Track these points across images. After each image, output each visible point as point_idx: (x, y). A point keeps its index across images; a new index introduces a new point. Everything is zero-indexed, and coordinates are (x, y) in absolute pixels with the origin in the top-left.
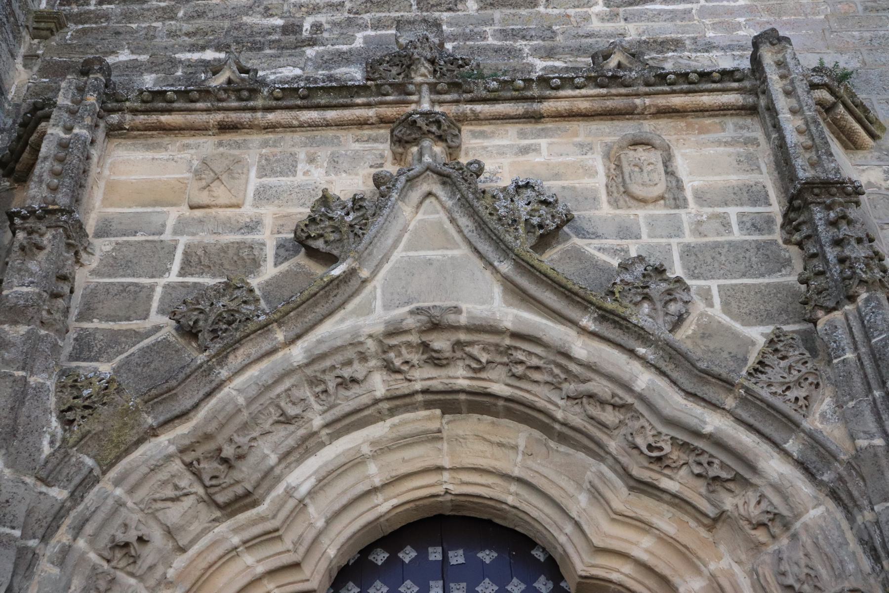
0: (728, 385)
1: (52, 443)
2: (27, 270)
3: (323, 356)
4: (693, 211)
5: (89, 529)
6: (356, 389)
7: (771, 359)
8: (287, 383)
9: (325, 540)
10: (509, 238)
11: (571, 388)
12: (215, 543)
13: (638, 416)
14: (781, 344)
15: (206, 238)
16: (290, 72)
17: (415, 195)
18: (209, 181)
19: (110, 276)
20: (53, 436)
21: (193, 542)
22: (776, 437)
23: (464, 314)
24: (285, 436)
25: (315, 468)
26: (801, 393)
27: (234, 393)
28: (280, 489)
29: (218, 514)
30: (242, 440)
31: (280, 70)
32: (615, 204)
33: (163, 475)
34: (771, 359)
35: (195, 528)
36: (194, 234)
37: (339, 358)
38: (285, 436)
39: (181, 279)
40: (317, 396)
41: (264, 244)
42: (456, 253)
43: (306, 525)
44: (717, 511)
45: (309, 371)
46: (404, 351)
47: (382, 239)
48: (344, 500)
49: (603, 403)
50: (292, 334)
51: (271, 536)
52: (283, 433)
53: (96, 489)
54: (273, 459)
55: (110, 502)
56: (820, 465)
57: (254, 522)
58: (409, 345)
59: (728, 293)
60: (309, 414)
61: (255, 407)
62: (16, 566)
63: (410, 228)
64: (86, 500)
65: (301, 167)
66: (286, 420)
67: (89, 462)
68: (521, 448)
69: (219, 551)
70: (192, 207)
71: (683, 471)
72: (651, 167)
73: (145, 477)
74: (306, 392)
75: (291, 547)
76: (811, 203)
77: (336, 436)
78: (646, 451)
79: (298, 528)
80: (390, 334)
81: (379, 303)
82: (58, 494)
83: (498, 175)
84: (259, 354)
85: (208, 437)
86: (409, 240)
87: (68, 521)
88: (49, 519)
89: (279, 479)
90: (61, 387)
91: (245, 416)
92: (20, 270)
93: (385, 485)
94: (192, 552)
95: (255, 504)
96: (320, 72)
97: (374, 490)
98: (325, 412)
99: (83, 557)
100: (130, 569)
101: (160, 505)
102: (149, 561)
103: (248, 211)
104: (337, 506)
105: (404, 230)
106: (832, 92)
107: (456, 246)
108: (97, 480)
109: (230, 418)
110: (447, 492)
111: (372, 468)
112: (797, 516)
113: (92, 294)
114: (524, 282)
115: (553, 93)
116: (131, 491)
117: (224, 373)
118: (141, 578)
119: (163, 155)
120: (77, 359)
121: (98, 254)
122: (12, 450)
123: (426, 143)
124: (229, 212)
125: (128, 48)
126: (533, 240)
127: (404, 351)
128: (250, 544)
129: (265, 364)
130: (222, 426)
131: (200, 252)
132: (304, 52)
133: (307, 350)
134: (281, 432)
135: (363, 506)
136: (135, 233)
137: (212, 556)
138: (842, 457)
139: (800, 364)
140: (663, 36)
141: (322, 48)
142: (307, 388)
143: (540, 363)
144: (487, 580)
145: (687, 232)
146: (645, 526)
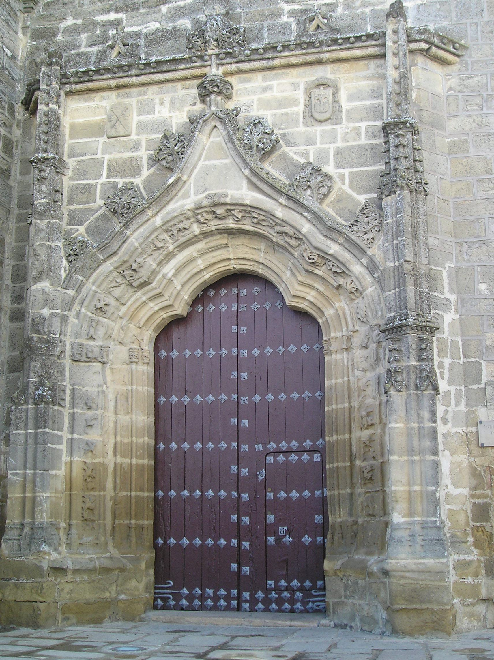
0: (340, 233)
1: (65, 271)
2: (42, 191)
3: (170, 221)
4: (344, 126)
5: (86, 303)
6: (186, 232)
7: (361, 218)
8: (156, 234)
9: (182, 293)
10: (248, 158)
11: (278, 228)
12: (137, 300)
13: (304, 243)
14: (367, 210)
15: (118, 156)
16: (154, 26)
17: (208, 128)
18: (115, 122)
19: (77, 180)
20: (65, 268)
21: (127, 301)
22: (358, 256)
23: (229, 197)
24: (159, 256)
25: (174, 265)
26: (370, 236)
27: (134, 240)
28: (160, 276)
29: (136, 289)
30: (139, 260)
31: (149, 24)
32: (306, 124)
33: (111, 278)
34: (361, 218)
36: (111, 153)
37: (177, 220)
38: (159, 256)
39: (108, 180)
41: (142, 158)
43: (173, 288)
44: (337, 284)
45: (164, 228)
46: (204, 214)
47: (192, 158)
48: (188, 276)
49: (291, 237)
50: (154, 212)
51: (159, 295)
52: (157, 254)
53: (85, 287)
54: (154, 266)
55: (91, 292)
56: (374, 270)
58: (206, 212)
59: (353, 176)
61: (144, 245)
62: (61, 323)
63: (206, 148)
64: (82, 292)
65: (157, 108)
67: (81, 278)
68: (263, 250)
69: (138, 303)
70: (108, 138)
71: (324, 267)
72: (325, 100)
73: (103, 281)
74: (166, 236)
76: (390, 133)
78: (307, 260)
79: (170, 290)
80: (197, 209)
82: (71, 292)
83: (251, 108)
84: (142, 222)
85: (125, 262)
86: (206, 155)
87: (77, 301)
89: (159, 272)
90: (65, 245)
91: (140, 250)
92: (39, 191)
93: (205, 268)
94: (128, 304)
95: (150, 283)
96: (169, 25)
97: (201, 271)
99: (85, 315)
100: (104, 316)
101: (112, 289)
102: (111, 311)
104: (185, 279)
105: (204, 149)
106: (426, 42)
107: (227, 157)
109: (133, 252)
110: (234, 267)
111: (200, 261)
112: (364, 290)
113: (73, 189)
114: (255, 180)
115: (279, 55)
116: (99, 287)
117: (128, 233)
118: (108, 318)
119: (91, 104)
120: (70, 225)
121: (71, 168)
123: (213, 97)
124: (125, 139)
125: (71, 15)
127: (204, 214)
128: (151, 299)
129: (145, 226)
130: (131, 256)
131: (115, 164)
132: (161, 9)
133: (162, 219)
134: (156, 253)
136: (85, 155)
137: (136, 306)
138: (381, 268)
139: (373, 221)
141: (170, 5)
142: (165, 234)
143: (264, 218)
145: (339, 139)
146: (312, 288)
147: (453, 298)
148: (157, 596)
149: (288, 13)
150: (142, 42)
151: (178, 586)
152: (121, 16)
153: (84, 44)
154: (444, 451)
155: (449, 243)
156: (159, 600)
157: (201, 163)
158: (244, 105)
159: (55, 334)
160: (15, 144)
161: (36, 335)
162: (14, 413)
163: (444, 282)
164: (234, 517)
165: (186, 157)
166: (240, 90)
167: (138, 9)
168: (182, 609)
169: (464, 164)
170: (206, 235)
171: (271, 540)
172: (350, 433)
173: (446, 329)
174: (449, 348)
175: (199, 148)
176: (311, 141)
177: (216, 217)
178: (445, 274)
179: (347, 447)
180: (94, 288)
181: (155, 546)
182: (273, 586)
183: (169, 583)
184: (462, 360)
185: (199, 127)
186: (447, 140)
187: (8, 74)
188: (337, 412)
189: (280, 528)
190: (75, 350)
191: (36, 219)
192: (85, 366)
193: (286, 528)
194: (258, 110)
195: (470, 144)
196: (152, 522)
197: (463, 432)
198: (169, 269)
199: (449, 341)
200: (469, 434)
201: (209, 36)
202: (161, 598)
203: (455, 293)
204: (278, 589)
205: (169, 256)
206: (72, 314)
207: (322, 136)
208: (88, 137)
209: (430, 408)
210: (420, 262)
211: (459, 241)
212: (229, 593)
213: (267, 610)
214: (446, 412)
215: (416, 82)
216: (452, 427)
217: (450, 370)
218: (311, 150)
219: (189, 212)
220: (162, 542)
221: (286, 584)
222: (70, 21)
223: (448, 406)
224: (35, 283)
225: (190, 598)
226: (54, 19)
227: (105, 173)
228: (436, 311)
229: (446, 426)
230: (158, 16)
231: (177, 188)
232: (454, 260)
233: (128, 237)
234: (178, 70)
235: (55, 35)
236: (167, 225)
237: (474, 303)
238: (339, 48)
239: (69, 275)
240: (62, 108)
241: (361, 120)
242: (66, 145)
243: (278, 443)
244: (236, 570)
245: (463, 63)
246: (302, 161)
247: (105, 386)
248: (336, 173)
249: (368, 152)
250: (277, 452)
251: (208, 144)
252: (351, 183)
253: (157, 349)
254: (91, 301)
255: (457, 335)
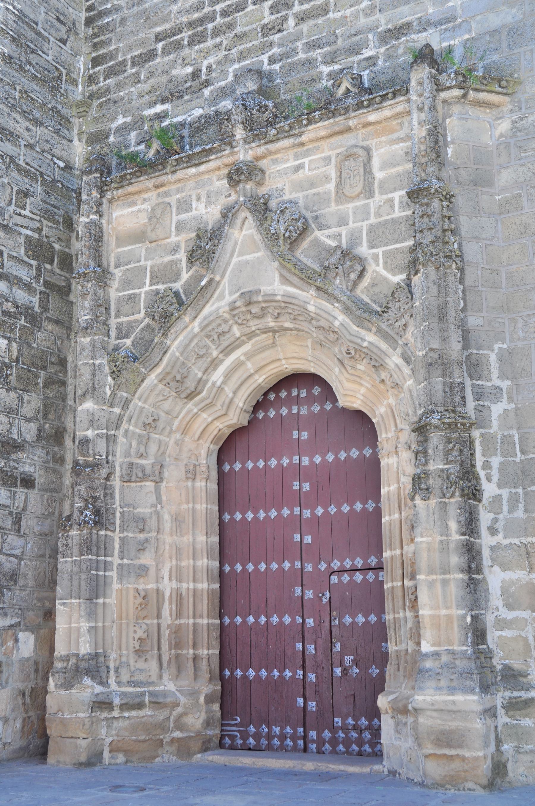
1: (110, 388)
3: (207, 325)
5: (133, 421)
6: (227, 336)
8: (195, 341)
9: (236, 400)
15: (159, 261)
16: (198, 112)
20: (110, 386)
24: (203, 363)
28: (209, 384)
29: (186, 400)
31: (193, 112)
33: (156, 392)
35: (178, 408)
36: (153, 259)
37: (214, 325)
38: (203, 363)
39: (151, 288)
40: (211, 341)
42: (259, 254)
51: (210, 405)
53: (132, 403)
54: (200, 375)
57: (202, 400)
60: (210, 351)
61: (185, 354)
63: (239, 242)
66: (200, 357)
67: (125, 395)
69: (190, 416)
75: (220, 408)
77: (227, 355)
81: (227, 292)
82: (117, 410)
85: (168, 374)
87: (125, 419)
88: (116, 422)
89: (207, 381)
90: (109, 362)
93: (256, 372)
94: (180, 417)
98: (217, 348)
99: (134, 433)
100: (154, 432)
101: (158, 404)
102: (161, 427)
103: (174, 239)
105: (236, 243)
107: (259, 250)
108: (131, 401)
109: (175, 363)
110: (286, 368)
113: (119, 301)
122: (95, 397)
126: (288, 246)
127: (241, 316)
128: (203, 410)
133: (200, 324)
135: (246, 385)
137: (188, 419)
140: (401, 21)
141: (212, 87)
144: (316, 404)
145: (372, 214)
147: (505, 384)
148: (225, 733)
149: (327, 75)
150: (186, 132)
151: (245, 724)
152: (167, 106)
153: (133, 142)
154: (492, 566)
155: (500, 320)
156: (227, 738)
157: (235, 260)
158: (277, 189)
159: (100, 456)
160: (74, 258)
161: (82, 458)
162: (61, 540)
163: (492, 367)
164: (299, 646)
165: (217, 255)
166: (273, 173)
167: (182, 97)
168: (250, 749)
169: (518, 223)
170: (251, 335)
171: (338, 671)
172: (402, 548)
173: (495, 422)
174: (499, 444)
175: (229, 246)
176: (343, 222)
177: (254, 317)
178: (493, 357)
179: (399, 565)
180: (140, 404)
181: (222, 677)
182: (340, 724)
183: (236, 720)
184: (519, 457)
185: (228, 221)
186: (497, 198)
187: (60, 186)
188: (390, 524)
189: (346, 657)
190: (124, 470)
191: (80, 337)
192: (136, 486)
193: (352, 657)
194: (290, 193)
195: (524, 199)
196: (217, 652)
197: (521, 543)
198: (217, 376)
199: (499, 437)
200: (529, 545)
201: (235, 120)
202: (229, 736)
203: (508, 378)
204: (345, 728)
205: (214, 364)
206: (120, 433)
207: (354, 213)
208: (132, 245)
209: (458, 519)
210: (450, 348)
211: (513, 316)
212: (295, 731)
213: (334, 752)
214: (495, 520)
215: (451, 136)
216: (505, 538)
217: (500, 470)
218: (344, 231)
219: (225, 315)
220: (229, 673)
221: (353, 722)
222: (121, 120)
223: (498, 514)
224: (81, 404)
225: (257, 736)
226: (106, 120)
227: (148, 281)
228: (480, 402)
229: (496, 537)
230: (201, 101)
231: (211, 289)
232: (507, 339)
233: (169, 348)
234: (210, 160)
235: (107, 137)
236: (206, 331)
237: (531, 389)
238: (365, 111)
239: (114, 394)
240: (105, 217)
241: (395, 190)
242: (113, 255)
243: (342, 561)
244: (302, 705)
245: (515, 102)
246: (334, 244)
247: (159, 506)
248: (370, 254)
249: (402, 225)
250: (342, 571)
251: (241, 237)
252: (385, 263)
253: (220, 462)
254: (138, 418)
255: (512, 428)
